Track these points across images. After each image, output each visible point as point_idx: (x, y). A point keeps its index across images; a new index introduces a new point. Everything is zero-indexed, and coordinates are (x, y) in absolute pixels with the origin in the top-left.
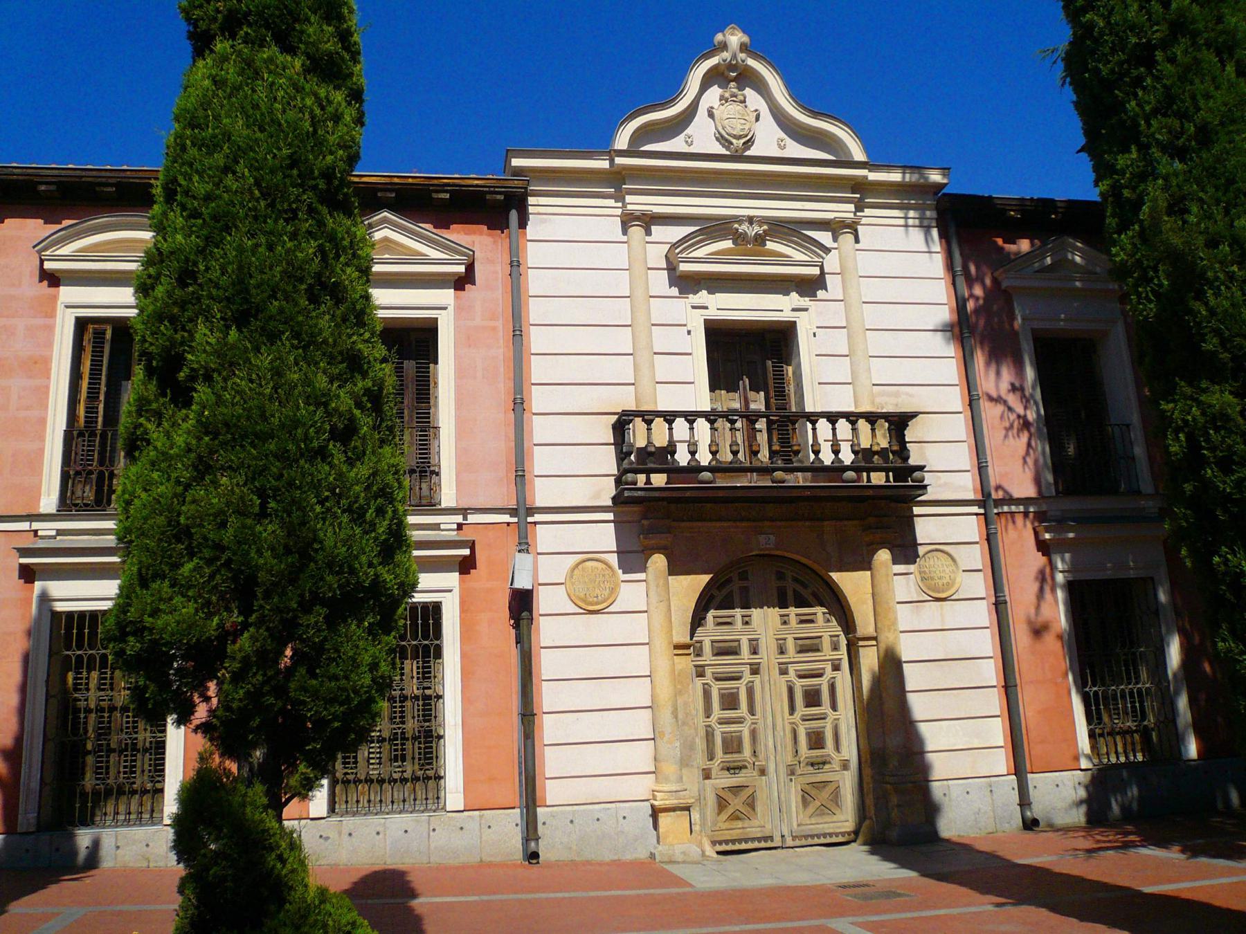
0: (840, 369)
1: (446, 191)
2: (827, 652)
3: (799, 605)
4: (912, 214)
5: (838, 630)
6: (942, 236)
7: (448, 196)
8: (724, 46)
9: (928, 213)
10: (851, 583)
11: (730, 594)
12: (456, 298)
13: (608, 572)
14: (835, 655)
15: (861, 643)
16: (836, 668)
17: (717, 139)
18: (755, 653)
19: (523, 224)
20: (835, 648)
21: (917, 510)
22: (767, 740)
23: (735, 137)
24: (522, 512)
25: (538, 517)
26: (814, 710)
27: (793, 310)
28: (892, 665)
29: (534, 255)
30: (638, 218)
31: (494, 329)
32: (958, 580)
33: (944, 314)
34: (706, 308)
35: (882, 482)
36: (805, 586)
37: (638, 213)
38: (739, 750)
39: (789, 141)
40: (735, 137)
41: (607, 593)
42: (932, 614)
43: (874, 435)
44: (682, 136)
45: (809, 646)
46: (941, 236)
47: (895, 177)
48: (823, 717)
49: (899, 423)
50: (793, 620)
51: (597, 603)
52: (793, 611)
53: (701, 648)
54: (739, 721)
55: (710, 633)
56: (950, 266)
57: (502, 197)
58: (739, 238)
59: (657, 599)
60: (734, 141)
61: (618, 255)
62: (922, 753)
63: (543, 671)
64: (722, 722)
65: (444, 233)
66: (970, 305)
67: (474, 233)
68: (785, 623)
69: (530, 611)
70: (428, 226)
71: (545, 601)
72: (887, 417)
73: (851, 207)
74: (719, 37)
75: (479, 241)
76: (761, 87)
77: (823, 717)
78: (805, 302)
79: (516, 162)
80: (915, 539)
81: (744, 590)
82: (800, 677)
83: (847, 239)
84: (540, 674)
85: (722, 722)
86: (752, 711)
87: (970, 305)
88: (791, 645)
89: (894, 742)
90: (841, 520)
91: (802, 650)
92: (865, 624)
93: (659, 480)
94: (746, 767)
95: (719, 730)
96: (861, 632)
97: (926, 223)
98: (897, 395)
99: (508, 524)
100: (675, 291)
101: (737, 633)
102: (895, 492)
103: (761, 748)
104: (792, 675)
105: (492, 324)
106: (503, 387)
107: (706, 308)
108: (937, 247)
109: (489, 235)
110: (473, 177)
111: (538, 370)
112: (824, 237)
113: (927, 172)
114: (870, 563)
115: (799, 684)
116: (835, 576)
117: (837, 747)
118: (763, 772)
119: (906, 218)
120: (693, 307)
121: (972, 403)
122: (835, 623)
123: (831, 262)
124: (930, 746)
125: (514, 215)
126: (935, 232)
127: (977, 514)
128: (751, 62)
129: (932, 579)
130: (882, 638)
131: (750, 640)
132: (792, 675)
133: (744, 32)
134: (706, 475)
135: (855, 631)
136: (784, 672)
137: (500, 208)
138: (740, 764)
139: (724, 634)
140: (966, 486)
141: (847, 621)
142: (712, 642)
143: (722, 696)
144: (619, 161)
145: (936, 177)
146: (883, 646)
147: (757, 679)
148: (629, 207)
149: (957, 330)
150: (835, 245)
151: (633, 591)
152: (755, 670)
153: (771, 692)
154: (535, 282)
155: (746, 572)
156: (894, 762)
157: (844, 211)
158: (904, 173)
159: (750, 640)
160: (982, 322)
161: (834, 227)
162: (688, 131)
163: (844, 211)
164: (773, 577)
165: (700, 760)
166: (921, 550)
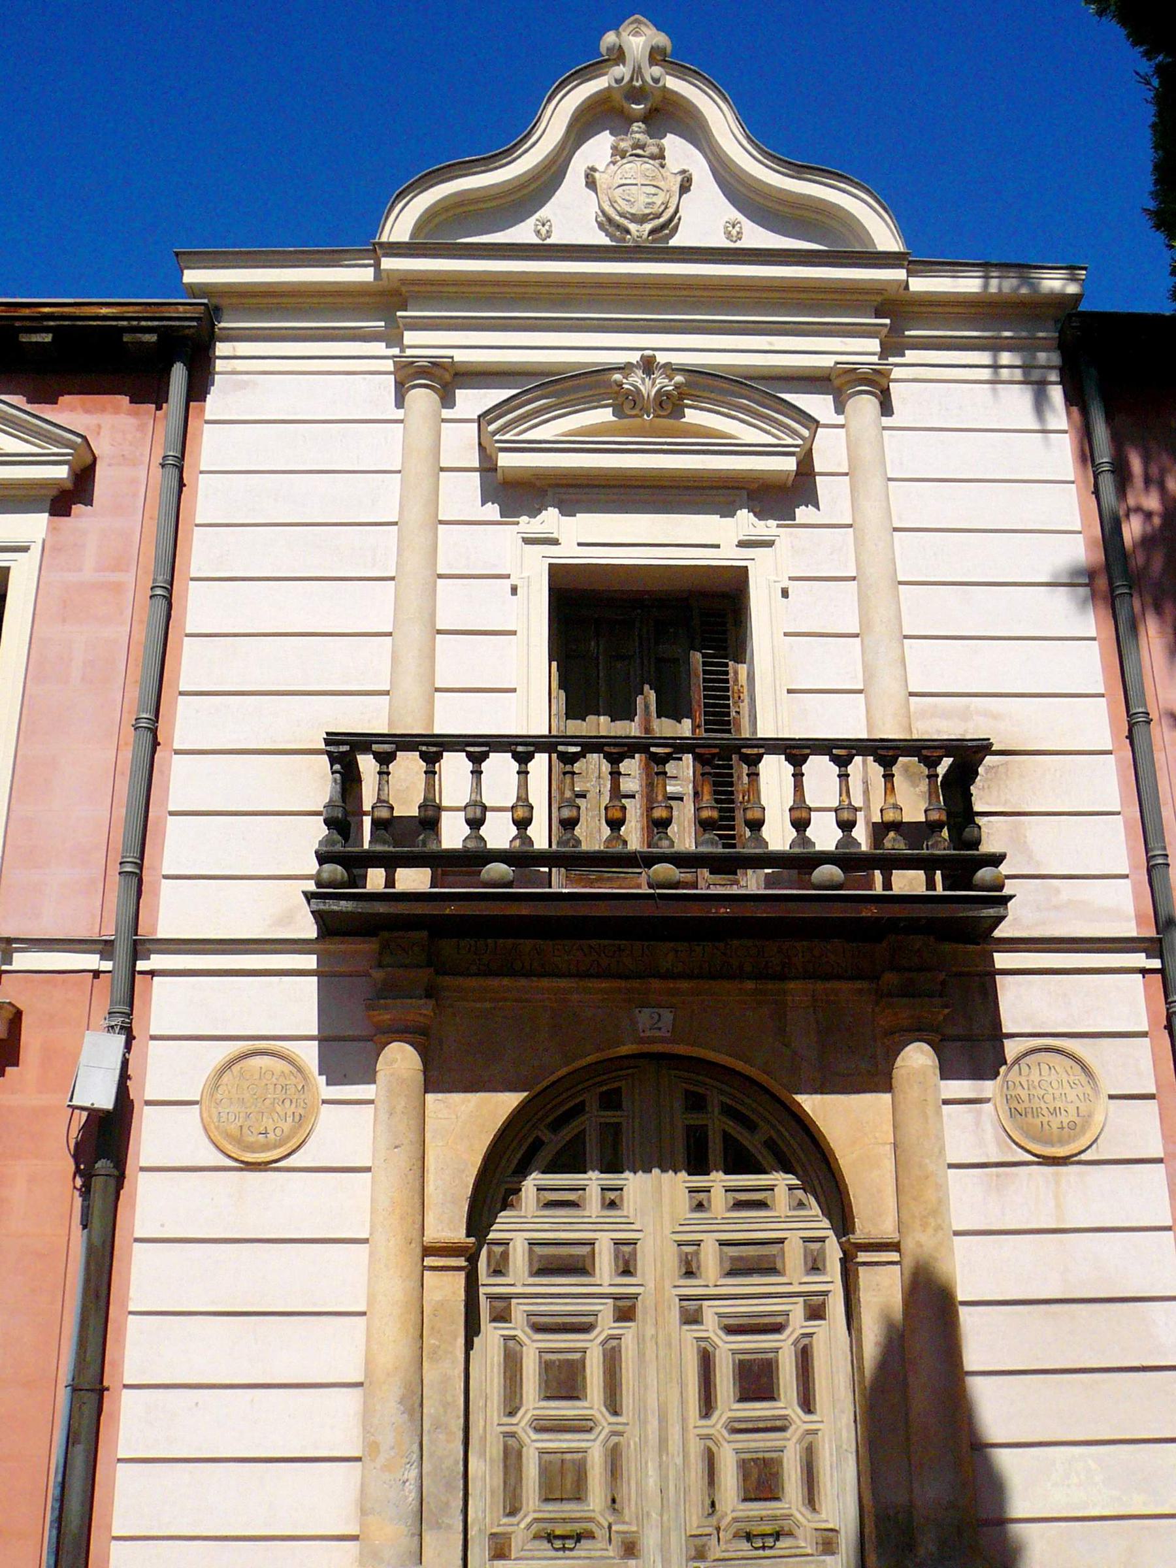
0: (840, 664)
1: (47, 330)
2: (795, 1275)
3: (731, 1169)
4: (1006, 358)
5: (823, 1226)
6: (1073, 398)
7: (48, 338)
8: (619, 55)
9: (1042, 357)
11: (580, 1138)
12: (51, 529)
13: (295, 1080)
14: (815, 1283)
16: (816, 1312)
17: (601, 226)
18: (627, 1272)
19: (198, 389)
20: (815, 1266)
21: (1002, 960)
22: (645, 1477)
23: (634, 218)
24: (122, 950)
25: (156, 961)
26: (759, 1410)
27: (742, 544)
28: (932, 1307)
29: (213, 446)
30: (423, 372)
31: (118, 588)
32: (1099, 1118)
33: (1077, 549)
34: (555, 542)
35: (921, 890)
36: (751, 1127)
37: (423, 362)
38: (578, 1495)
39: (748, 226)
40: (634, 218)
41: (286, 1126)
42: (1034, 1194)
43: (890, 787)
44: (531, 221)
45: (754, 1262)
46: (1070, 400)
47: (969, 284)
48: (779, 1427)
49: (959, 765)
50: (719, 1200)
51: (266, 1147)
52: (718, 1180)
53: (505, 1256)
54: (583, 1426)
55: (524, 1224)
56: (1086, 455)
57: (153, 338)
58: (626, 403)
59: (390, 1146)
60: (633, 227)
61: (386, 446)
62: (1001, 1522)
63: (132, 1293)
64: (543, 1427)
65: (47, 411)
66: (1133, 529)
67: (103, 410)
68: (700, 1206)
69: (120, 1164)
70: (18, 400)
71: (155, 1137)
72: (926, 751)
73: (874, 345)
74: (610, 38)
75: (113, 429)
76: (694, 129)
77: (779, 1427)
78: (768, 528)
79: (192, 276)
81: (612, 1134)
82: (731, 1330)
83: (865, 405)
84: (125, 1299)
85: (543, 1427)
86: (614, 1408)
87: (1133, 529)
88: (710, 1259)
89: (931, 1491)
90: (828, 977)
91: (737, 1270)
92: (875, 1215)
93: (413, 880)
94: (590, 1536)
95: (534, 1445)
96: (864, 1230)
97: (1036, 375)
98: (965, 715)
99: (96, 974)
100: (492, 511)
101: (590, 1225)
102: (943, 911)
103: (629, 1492)
105: (117, 577)
106: (120, 699)
107: (555, 542)
108: (1059, 415)
109: (135, 414)
110: (102, 300)
111: (193, 665)
112: (818, 405)
113: (1035, 274)
114: (889, 1076)
115: (727, 1348)
116: (809, 1103)
117: (811, 1500)
118: (630, 1549)
119: (996, 367)
120: (528, 541)
121: (1135, 726)
122: (816, 1210)
123: (829, 452)
124: (1020, 1505)
125: (178, 374)
126: (1056, 394)
127: (1144, 971)
128: (673, 83)
129: (1037, 1113)
130: (908, 1245)
133: (659, 27)
134: (499, 869)
136: (692, 1318)
137: (158, 360)
138: (578, 1527)
139: (560, 1227)
140: (1120, 909)
142: (532, 1244)
143: (547, 1367)
144: (388, 263)
145: (1054, 283)
146: (908, 1262)
147: (629, 1332)
148: (409, 352)
149: (1102, 582)
150: (840, 420)
151: (352, 1125)
153: (659, 1361)
154: (208, 498)
155: (618, 1091)
156: (927, 1546)
157: (863, 350)
158: (986, 278)
159: (617, 1243)
160: (1157, 564)
161: (835, 383)
162: (542, 213)
163: (863, 350)
164: (677, 1105)
165: (485, 1511)
166: (1012, 1049)
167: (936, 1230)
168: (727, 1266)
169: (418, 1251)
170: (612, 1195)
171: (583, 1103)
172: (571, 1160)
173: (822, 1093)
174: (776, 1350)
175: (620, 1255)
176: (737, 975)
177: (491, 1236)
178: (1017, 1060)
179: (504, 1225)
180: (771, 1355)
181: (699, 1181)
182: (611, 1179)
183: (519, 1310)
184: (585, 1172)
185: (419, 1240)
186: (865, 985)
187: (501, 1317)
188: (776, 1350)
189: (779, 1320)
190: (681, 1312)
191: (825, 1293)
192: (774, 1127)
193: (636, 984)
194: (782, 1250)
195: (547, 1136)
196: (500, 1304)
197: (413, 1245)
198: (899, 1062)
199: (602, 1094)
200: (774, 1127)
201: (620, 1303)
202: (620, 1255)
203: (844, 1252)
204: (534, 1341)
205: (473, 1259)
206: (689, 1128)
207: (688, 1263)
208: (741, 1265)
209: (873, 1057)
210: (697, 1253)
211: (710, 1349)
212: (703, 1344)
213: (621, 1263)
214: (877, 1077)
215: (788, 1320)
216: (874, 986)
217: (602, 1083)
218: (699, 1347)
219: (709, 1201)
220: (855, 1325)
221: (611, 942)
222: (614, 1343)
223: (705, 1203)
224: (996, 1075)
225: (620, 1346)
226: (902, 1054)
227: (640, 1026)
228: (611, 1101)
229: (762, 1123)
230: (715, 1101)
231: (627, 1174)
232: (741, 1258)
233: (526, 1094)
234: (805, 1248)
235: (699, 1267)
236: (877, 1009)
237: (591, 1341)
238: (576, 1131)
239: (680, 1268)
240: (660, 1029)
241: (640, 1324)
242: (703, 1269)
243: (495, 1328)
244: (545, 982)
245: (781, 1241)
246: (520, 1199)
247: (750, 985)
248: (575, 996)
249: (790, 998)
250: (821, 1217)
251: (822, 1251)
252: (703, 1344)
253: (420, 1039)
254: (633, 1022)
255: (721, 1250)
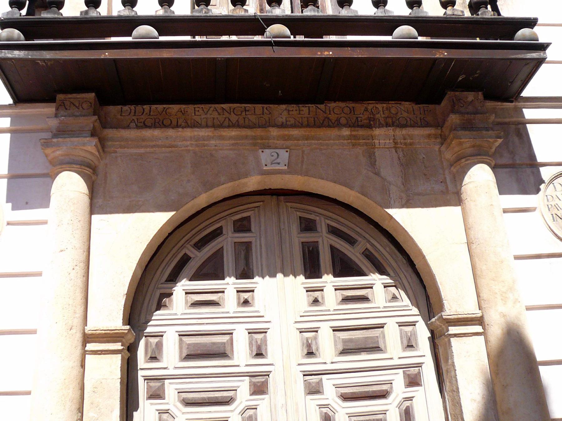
2: (394, 350)
5: (414, 313)
10: (423, 226)
11: (218, 255)
15: (453, 330)
16: (413, 381)
21: (529, 113)
36: (351, 241)
50: (331, 298)
52: (328, 281)
53: (159, 346)
68: (316, 301)
80: (532, 156)
82: (346, 398)
88: (327, 344)
90: (403, 126)
92: (457, 298)
104: (330, 394)
122: (406, 301)
131: (251, 332)
132: (330, 394)
135: (441, 308)
139: (205, 320)
141: (423, 290)
146: (496, 331)
152: (259, 389)
155: (248, 219)
159: (251, 332)
166: (546, 173)
167: (515, 303)
168: (341, 348)
169: (78, 337)
170: (246, 296)
171: (221, 228)
172: (212, 270)
173: (408, 207)
174: (384, 413)
175: (254, 343)
176: (338, 125)
177: (149, 330)
178: (551, 181)
179: (158, 321)
180: (381, 416)
181: (314, 282)
182: (245, 283)
183: (171, 389)
184: (224, 279)
185: (80, 328)
186: (432, 131)
187: (156, 395)
188: (384, 413)
189: (384, 387)
190: (305, 384)
191: (419, 365)
192: (369, 242)
193: (259, 132)
194: (383, 333)
195: (191, 251)
196: (154, 384)
197: (73, 331)
198: (467, 179)
199: (235, 222)
200: (369, 242)
201: (254, 380)
202: (254, 343)
203: (432, 332)
204: (183, 413)
205: (132, 349)
206: (304, 245)
207: (309, 346)
208: (351, 346)
209: (444, 182)
210: (315, 338)
211: (331, 413)
212: (325, 410)
213: (254, 348)
214: (449, 194)
215: (391, 388)
216: (439, 132)
217: (236, 213)
218: (321, 413)
219: (323, 298)
220: (447, 386)
221: (239, 105)
222: (251, 412)
223: (320, 299)
224: (538, 191)
225: (256, 415)
226: (469, 173)
227: (264, 162)
228: (243, 226)
229: (360, 239)
230: (322, 225)
231: (257, 279)
232: (351, 340)
233: (172, 213)
234: (401, 330)
235: (317, 349)
236: (443, 148)
237: (232, 411)
238: (214, 250)
239: (302, 350)
240: (279, 164)
241: (272, 394)
242: (321, 349)
243: (152, 404)
244: (188, 133)
245: (381, 326)
246: (171, 301)
247: (346, 132)
248: (213, 142)
249: (377, 141)
250: (411, 307)
251: (414, 334)
252: (325, 410)
253: (88, 171)
254: (258, 162)
255: (334, 336)
